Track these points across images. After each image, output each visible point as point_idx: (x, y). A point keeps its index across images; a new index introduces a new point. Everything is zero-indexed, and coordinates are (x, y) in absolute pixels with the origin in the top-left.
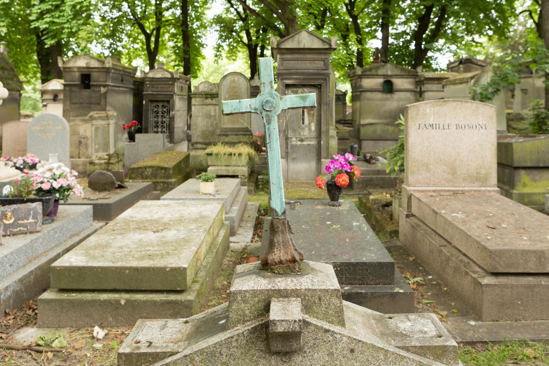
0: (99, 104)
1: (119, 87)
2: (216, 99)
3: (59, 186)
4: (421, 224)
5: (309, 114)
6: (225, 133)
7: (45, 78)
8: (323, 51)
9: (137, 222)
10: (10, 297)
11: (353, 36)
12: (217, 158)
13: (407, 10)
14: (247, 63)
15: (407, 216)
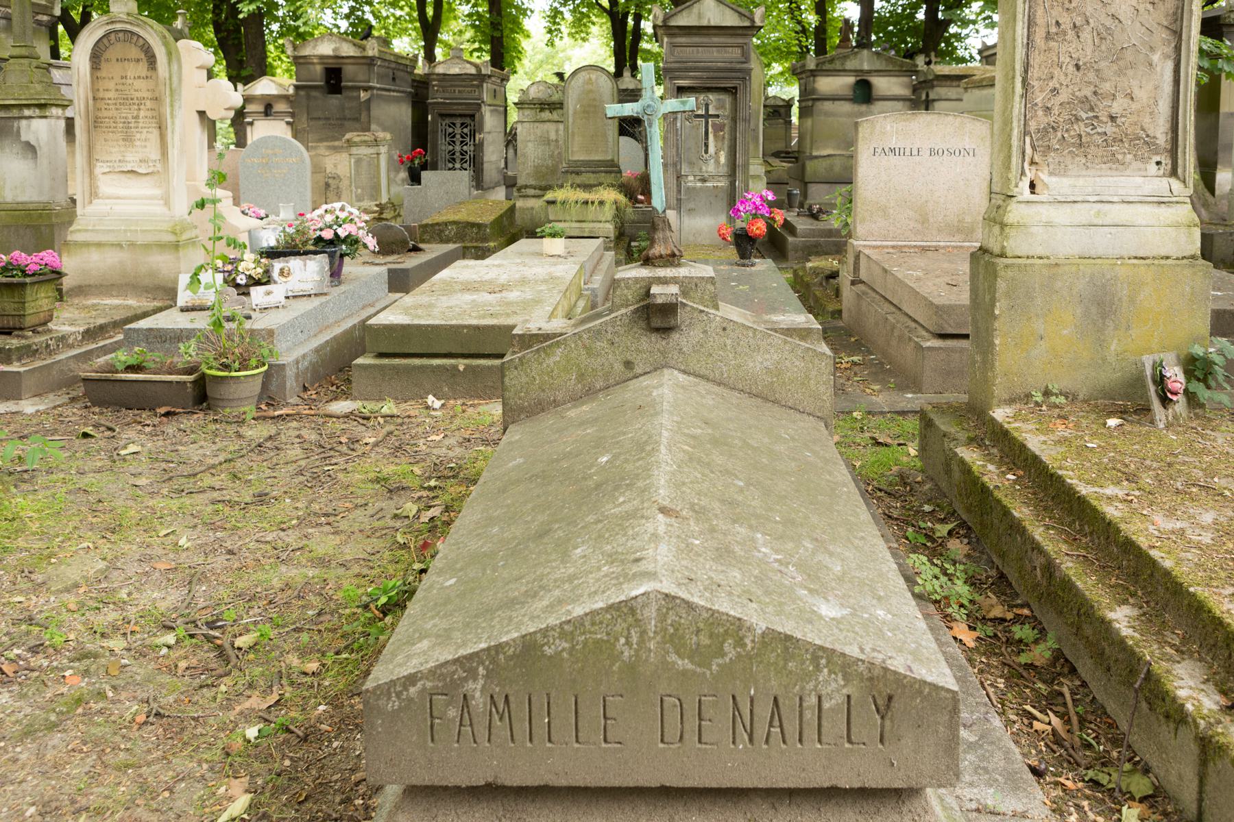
0: (357, 120)
1: (389, 90)
2: (560, 111)
3: (347, 233)
4: (869, 291)
5: (715, 136)
6: (575, 169)
7: (234, 73)
8: (740, 32)
9: (461, 283)
10: (307, 368)
12: (564, 209)
14: (608, 45)
15: (853, 283)
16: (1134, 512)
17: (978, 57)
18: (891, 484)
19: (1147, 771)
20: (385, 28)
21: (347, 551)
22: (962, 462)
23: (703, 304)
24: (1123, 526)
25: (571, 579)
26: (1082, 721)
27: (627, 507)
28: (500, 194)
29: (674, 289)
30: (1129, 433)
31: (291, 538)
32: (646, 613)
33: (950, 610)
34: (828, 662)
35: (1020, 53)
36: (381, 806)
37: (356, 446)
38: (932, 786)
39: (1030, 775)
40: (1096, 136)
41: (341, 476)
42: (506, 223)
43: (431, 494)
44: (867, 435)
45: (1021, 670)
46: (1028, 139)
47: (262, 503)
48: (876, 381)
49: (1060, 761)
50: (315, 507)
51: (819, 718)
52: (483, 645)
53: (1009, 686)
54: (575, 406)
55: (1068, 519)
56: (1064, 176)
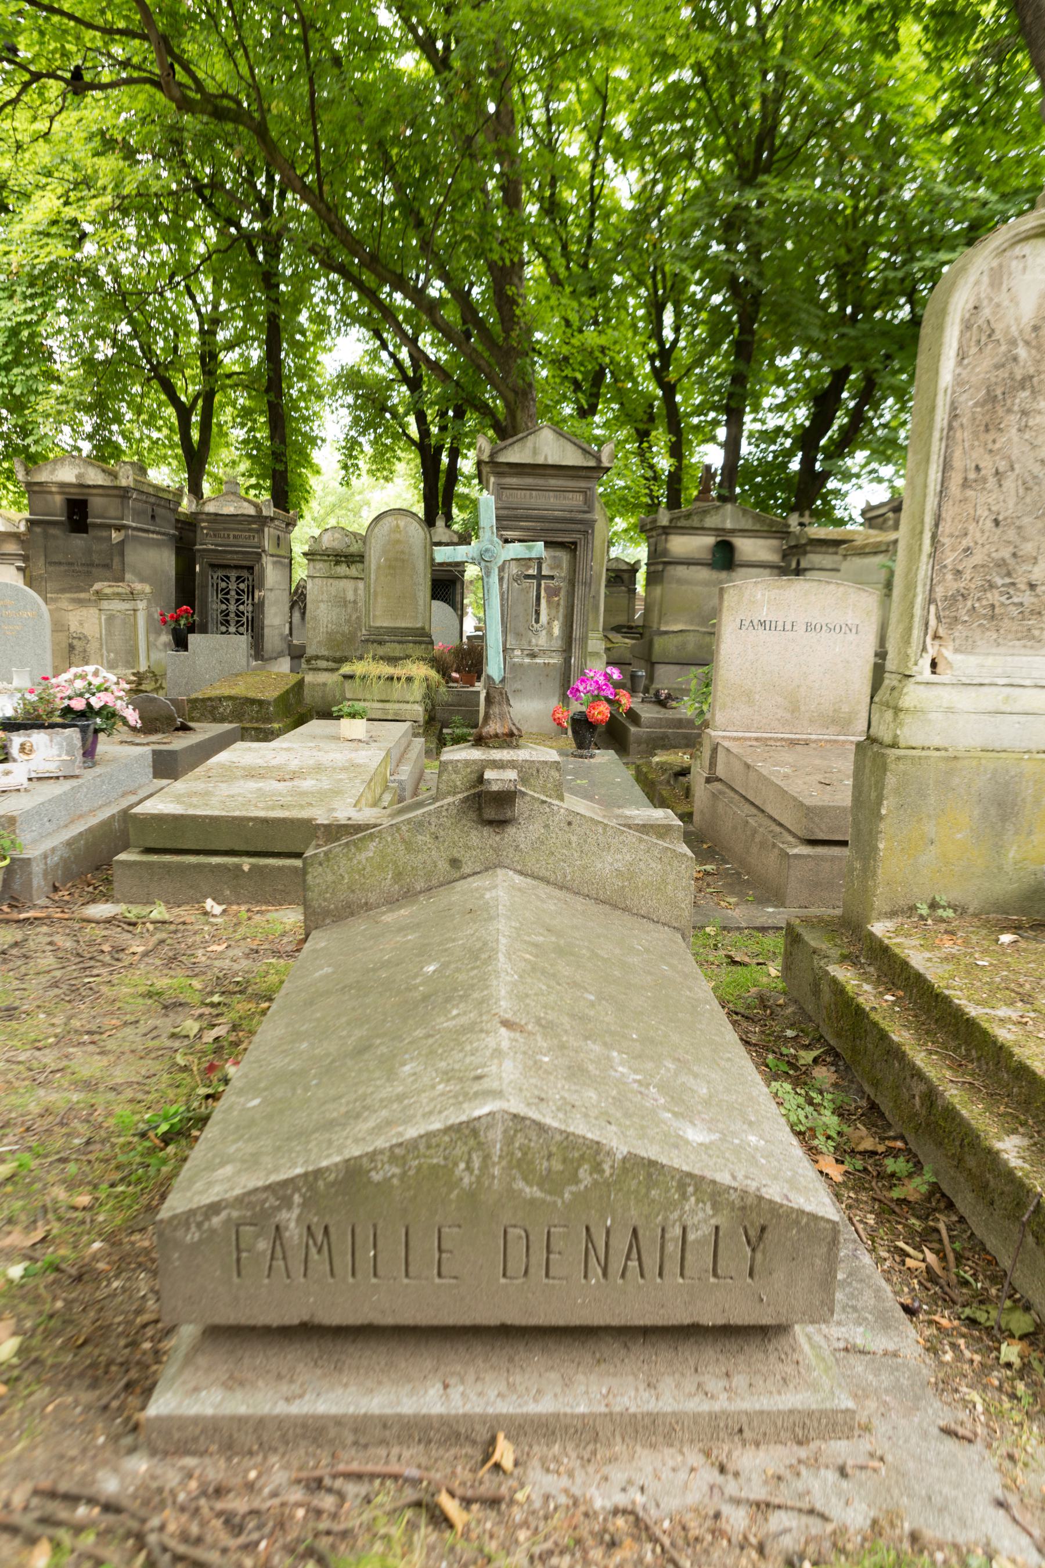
0: (107, 566)
2: (360, 566)
5: (549, 602)
6: (378, 638)
8: (583, 473)
11: (660, 438)
13: (791, 375)
15: (708, 780)
16: (1028, 1035)
17: (861, 520)
18: (748, 1007)
19: (1027, 1308)
20: (138, 453)
21: (117, 1073)
22: (834, 981)
23: (544, 793)
24: (1016, 1050)
25: (400, 1098)
26: (959, 1258)
27: (463, 1020)
28: (284, 665)
29: (512, 775)
30: (1025, 950)
31: (49, 1058)
32: (491, 1135)
33: (816, 1142)
34: (696, 1190)
35: (931, 503)
36: (175, 1349)
37: (121, 955)
38: (802, 1321)
39: (902, 1314)
40: (1012, 608)
41: (104, 989)
42: (292, 701)
43: (215, 1012)
44: (722, 953)
45: (893, 1205)
46: (933, 608)
47: (11, 1017)
48: (732, 893)
49: (934, 1299)
50: (76, 1023)
51: (683, 1250)
52: (299, 1171)
53: (880, 1222)
54: (391, 910)
55: (953, 1044)
56: (971, 653)
